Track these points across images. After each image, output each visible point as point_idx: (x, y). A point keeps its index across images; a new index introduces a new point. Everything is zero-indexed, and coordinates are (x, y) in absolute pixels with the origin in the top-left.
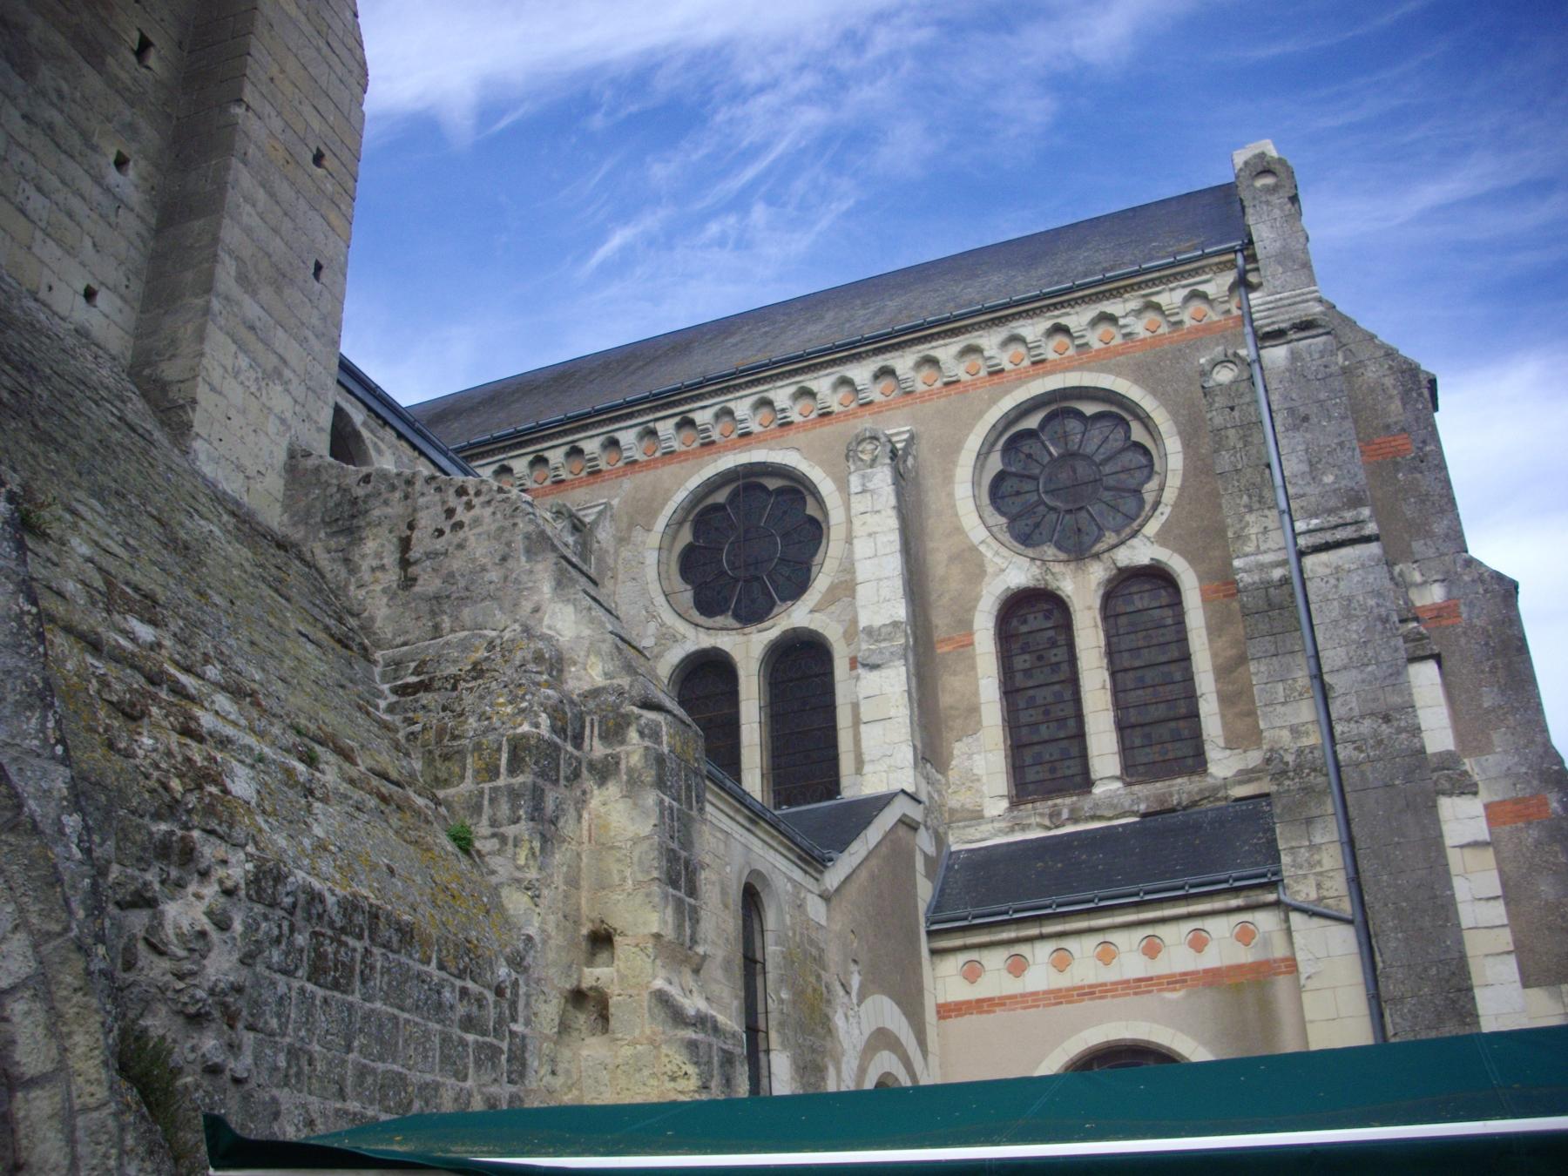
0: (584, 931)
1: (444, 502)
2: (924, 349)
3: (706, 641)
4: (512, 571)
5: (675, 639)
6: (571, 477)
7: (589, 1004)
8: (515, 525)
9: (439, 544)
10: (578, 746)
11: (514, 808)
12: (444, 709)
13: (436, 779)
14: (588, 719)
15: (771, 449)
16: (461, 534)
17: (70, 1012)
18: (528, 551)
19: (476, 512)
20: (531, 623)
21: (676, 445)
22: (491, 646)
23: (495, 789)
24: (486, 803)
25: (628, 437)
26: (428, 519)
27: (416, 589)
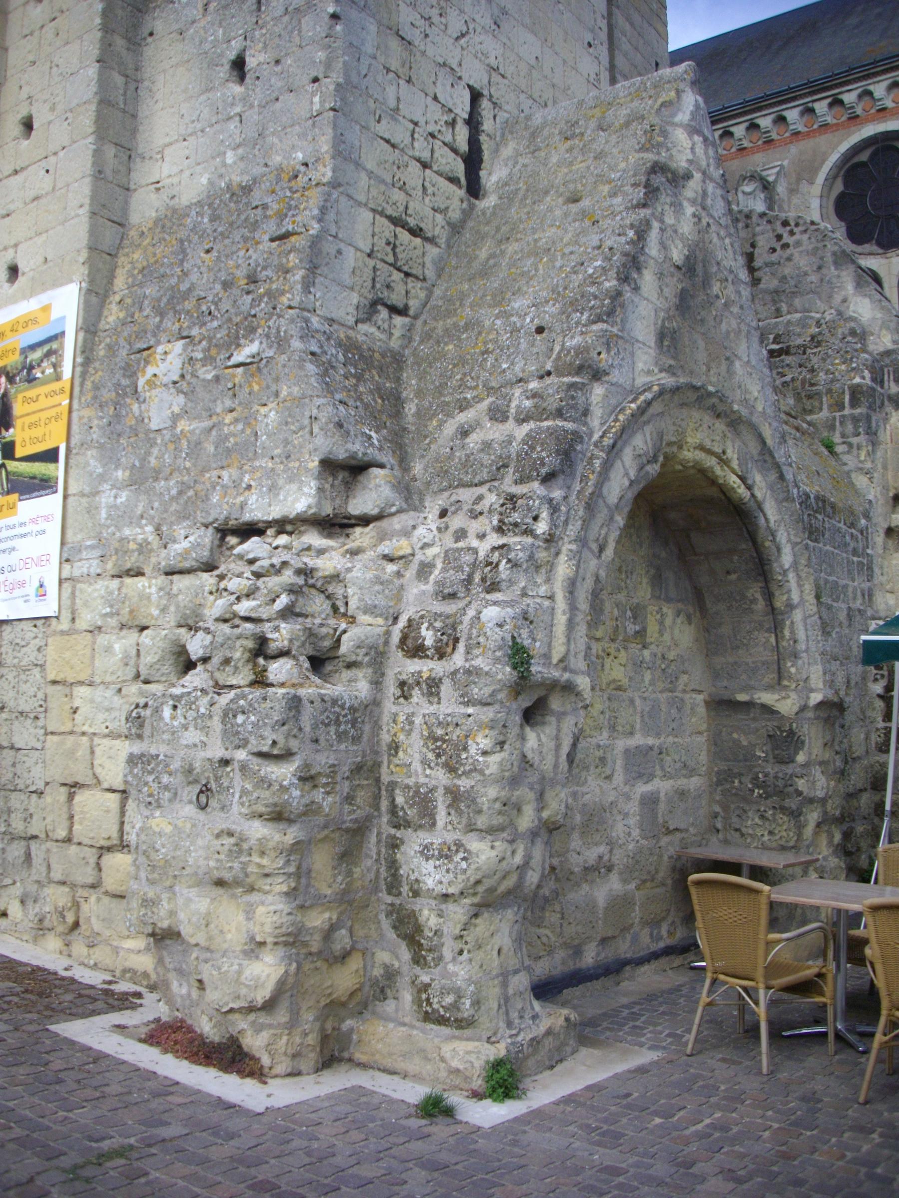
0: (891, 494)
1: (774, 231)
4: (826, 275)
6: (751, 145)
8: (825, 246)
9: (774, 257)
10: (882, 387)
11: (856, 427)
12: (800, 366)
13: (804, 410)
14: (886, 370)
16: (788, 252)
17: (803, 575)
18: (836, 263)
19: (797, 237)
20: (842, 309)
21: (829, 119)
22: (818, 324)
23: (843, 416)
24: (838, 424)
25: (792, 115)
26: (764, 242)
27: (761, 286)
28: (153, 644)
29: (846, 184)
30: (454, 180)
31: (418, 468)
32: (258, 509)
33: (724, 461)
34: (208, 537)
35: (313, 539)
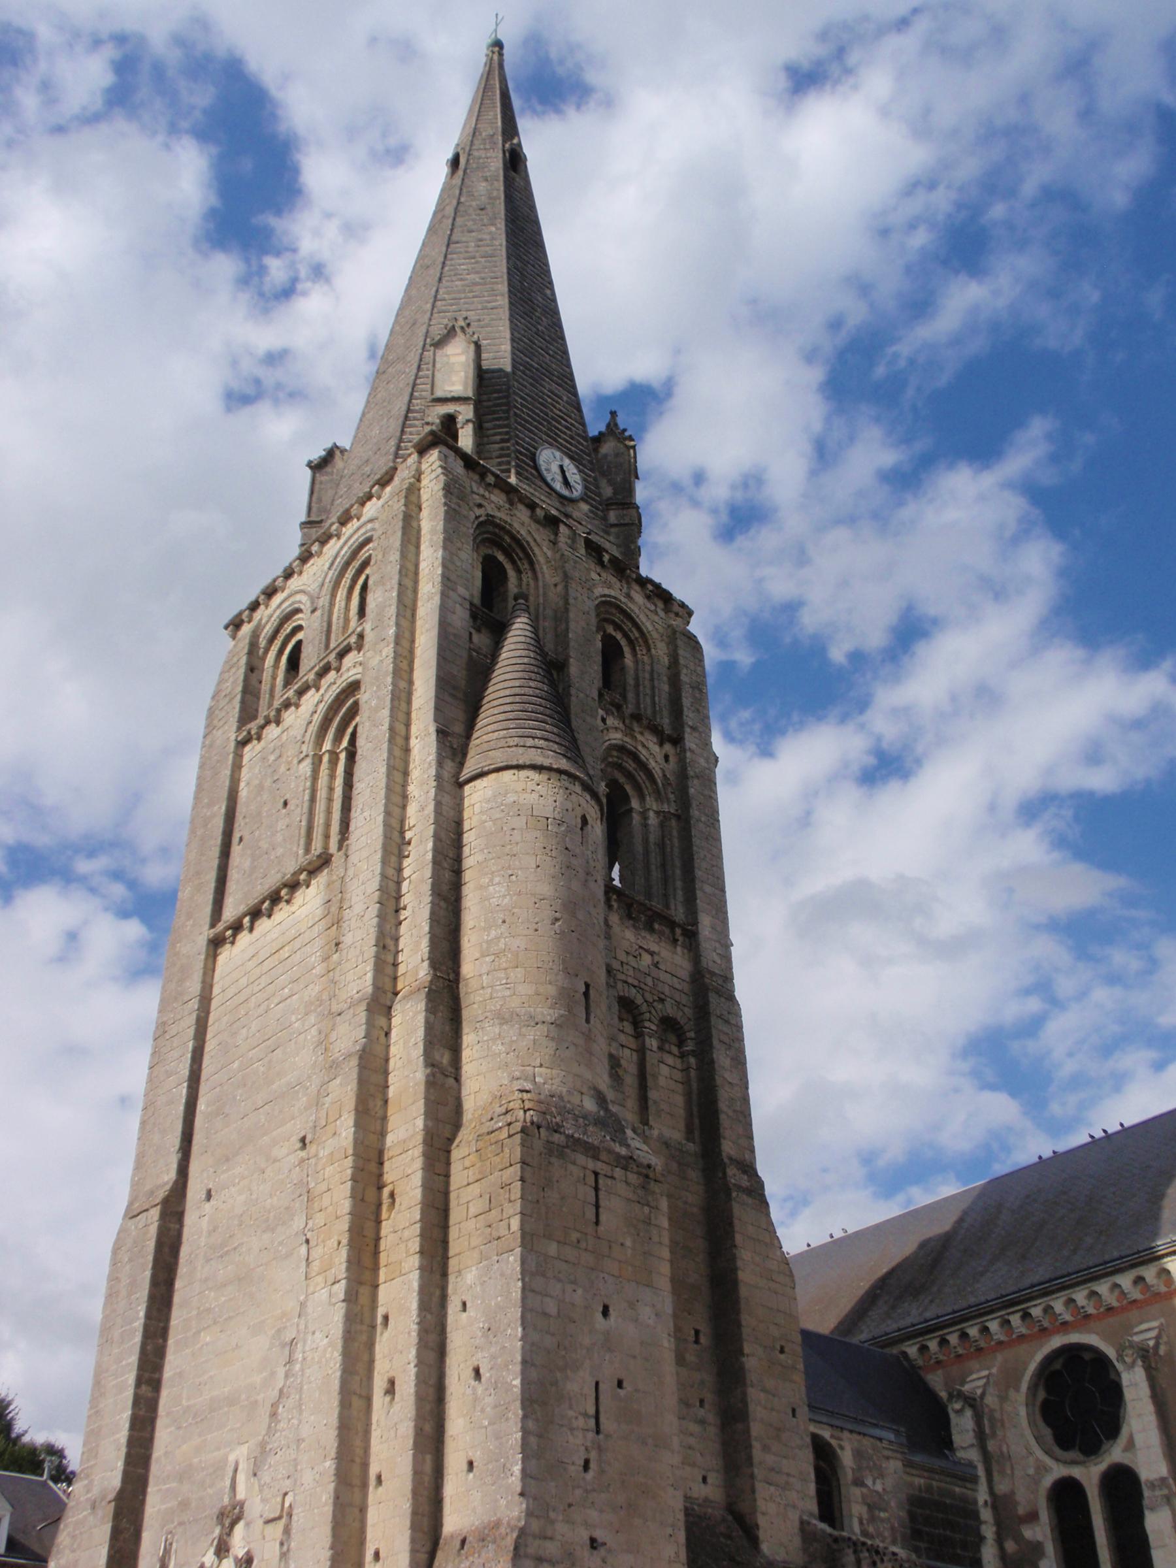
5: (1047, 1470)
15: (1081, 1333)
21: (1024, 1331)
29: (1048, 1390)
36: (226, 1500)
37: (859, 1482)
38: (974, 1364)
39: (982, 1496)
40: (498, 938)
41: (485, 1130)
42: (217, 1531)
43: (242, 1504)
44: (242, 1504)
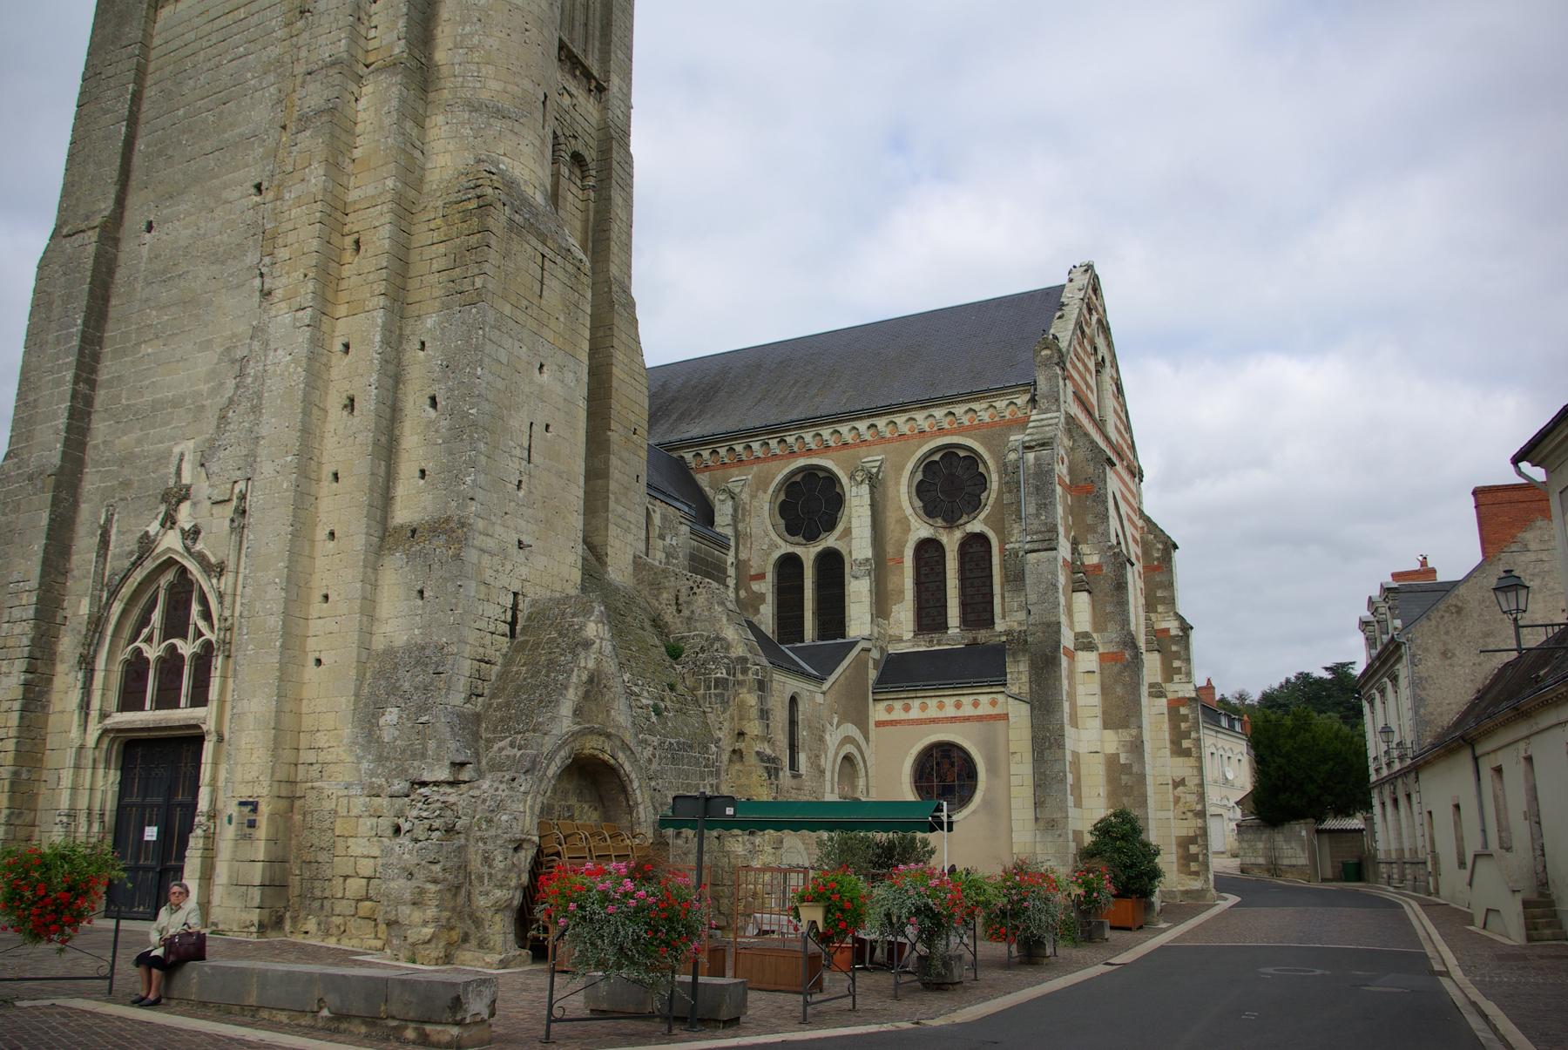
2: (891, 417)
3: (790, 549)
7: (737, 754)
28: (386, 824)
30: (504, 635)
31: (484, 762)
32: (426, 777)
33: (603, 751)
34: (408, 785)
35: (449, 790)
36: (171, 483)
37: (662, 537)
38: (735, 471)
39: (730, 559)
40: (472, 34)
41: (453, 198)
42: (163, 508)
43: (188, 488)
44: (188, 488)
